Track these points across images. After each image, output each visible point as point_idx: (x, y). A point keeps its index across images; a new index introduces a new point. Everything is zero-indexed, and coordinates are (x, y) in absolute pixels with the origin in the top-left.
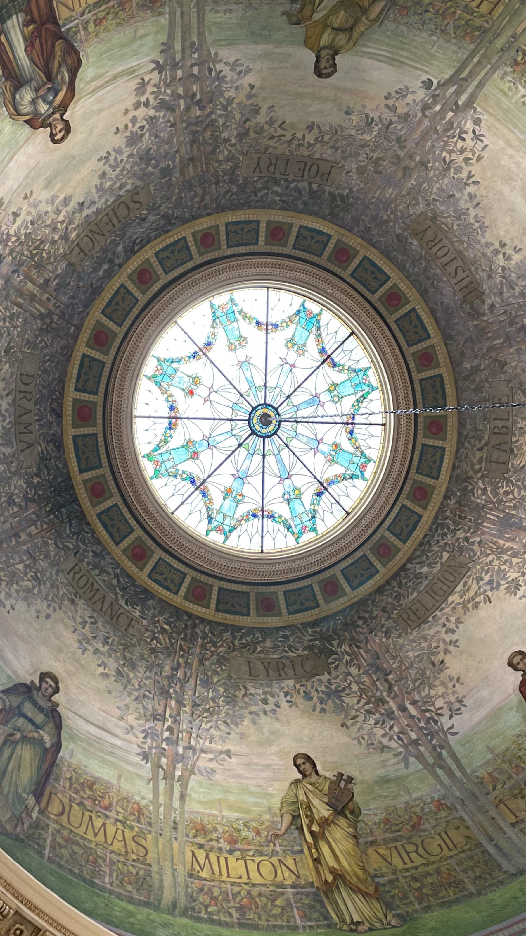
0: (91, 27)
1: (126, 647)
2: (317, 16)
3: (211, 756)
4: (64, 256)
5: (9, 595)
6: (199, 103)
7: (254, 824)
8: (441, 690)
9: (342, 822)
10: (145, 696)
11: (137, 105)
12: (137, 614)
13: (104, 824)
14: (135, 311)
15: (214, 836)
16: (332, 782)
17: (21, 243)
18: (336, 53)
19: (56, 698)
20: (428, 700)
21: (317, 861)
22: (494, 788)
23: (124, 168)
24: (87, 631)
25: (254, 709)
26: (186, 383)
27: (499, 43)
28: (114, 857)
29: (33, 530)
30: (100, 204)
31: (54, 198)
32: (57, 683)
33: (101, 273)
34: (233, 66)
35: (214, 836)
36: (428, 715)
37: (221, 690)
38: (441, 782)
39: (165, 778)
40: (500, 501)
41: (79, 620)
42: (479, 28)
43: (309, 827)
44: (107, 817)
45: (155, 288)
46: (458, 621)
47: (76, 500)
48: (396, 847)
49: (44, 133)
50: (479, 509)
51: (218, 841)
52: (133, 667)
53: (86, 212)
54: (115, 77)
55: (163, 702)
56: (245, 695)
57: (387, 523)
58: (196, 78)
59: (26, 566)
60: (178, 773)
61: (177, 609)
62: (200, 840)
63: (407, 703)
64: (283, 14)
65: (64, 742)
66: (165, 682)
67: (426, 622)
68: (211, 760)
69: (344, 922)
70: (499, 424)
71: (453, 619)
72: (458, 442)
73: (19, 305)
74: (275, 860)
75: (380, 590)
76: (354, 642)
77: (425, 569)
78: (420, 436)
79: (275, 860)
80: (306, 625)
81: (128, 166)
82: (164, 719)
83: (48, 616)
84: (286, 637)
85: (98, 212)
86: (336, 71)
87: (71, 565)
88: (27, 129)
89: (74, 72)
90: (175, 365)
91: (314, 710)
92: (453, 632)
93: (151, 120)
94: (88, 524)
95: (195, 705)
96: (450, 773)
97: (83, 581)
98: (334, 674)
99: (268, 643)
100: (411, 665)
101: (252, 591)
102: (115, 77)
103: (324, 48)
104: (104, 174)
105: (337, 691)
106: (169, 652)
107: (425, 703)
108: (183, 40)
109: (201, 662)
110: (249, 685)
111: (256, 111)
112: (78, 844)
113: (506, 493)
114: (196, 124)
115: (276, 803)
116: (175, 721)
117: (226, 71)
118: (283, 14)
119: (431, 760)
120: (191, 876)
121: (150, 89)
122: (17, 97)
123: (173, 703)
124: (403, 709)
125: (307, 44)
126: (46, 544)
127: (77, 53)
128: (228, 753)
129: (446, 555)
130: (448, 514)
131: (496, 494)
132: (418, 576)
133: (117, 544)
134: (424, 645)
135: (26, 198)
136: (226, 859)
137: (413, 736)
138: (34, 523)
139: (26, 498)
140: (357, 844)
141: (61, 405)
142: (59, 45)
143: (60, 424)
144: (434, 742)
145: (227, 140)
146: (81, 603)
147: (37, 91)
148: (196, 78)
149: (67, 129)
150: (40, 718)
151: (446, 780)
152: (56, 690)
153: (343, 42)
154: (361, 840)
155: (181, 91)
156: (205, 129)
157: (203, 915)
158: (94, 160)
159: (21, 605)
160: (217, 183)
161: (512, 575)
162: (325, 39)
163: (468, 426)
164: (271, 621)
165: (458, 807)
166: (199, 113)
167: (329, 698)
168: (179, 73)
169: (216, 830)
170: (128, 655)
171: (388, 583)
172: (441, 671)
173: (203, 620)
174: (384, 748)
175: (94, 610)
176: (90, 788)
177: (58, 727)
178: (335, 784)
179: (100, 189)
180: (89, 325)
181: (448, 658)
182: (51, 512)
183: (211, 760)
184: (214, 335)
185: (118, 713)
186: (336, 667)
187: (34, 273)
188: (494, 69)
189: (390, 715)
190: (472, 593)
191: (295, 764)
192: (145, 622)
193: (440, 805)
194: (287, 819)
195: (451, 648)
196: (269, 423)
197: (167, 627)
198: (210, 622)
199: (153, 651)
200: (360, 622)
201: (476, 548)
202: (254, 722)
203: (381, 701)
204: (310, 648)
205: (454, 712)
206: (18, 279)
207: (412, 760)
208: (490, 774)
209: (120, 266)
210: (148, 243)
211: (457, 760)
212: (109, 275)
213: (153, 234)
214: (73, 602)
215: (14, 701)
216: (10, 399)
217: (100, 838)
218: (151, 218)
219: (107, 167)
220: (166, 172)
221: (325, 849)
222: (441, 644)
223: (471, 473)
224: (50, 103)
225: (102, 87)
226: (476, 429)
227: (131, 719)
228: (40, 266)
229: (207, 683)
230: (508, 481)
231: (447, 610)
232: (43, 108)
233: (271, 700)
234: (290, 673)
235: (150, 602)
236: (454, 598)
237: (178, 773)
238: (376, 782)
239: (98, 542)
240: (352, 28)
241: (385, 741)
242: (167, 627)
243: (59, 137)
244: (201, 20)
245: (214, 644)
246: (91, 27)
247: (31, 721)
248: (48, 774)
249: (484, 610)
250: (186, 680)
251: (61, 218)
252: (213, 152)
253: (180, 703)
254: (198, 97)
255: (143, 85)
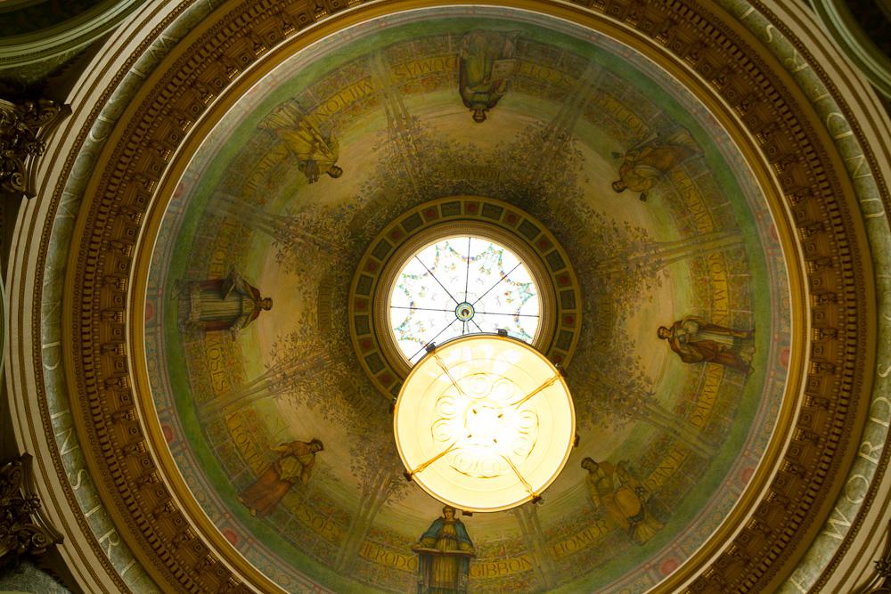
0: (695, 376)
1: (451, 162)
2: (615, 474)
3: (383, 142)
4: (611, 295)
5: (523, 140)
6: (620, 400)
7: (348, 124)
8: (291, 261)
9: (306, 158)
10: (429, 146)
11: (642, 374)
12: (454, 181)
13: (422, 71)
14: (560, 304)
15: (365, 104)
16: (319, 173)
17: (635, 280)
18: (591, 472)
19: (473, 113)
20: (294, 250)
21: (310, 128)
22: (242, 231)
23: (621, 348)
24: (474, 155)
25: (373, 181)
26: (511, 296)
27: (536, 543)
28: (412, 59)
29: (529, 177)
30: (616, 327)
31: (639, 309)
32: (476, 120)
33: (589, 304)
34: (623, 426)
35: (365, 104)
36: (290, 243)
37: (394, 177)
38: (267, 214)
39: (400, 115)
40: (331, 372)
41: (481, 156)
42: (550, 539)
43: (320, 143)
44: (423, 76)
45: (560, 320)
46: (305, 300)
47: (518, 206)
48: (274, 163)
49: (669, 324)
50: (337, 360)
51: (362, 103)
52: (442, 156)
53: (619, 318)
54: (663, 372)
55: (419, 150)
56: (381, 184)
57: (370, 318)
58: (630, 407)
59: (522, 159)
60: (395, 122)
61: (437, 198)
62: (370, 98)
63: (303, 241)
64: (629, 461)
65: (459, 95)
66: (422, 160)
67: (319, 288)
68: (382, 140)
69: (287, 106)
70: (362, 406)
71: (308, 299)
72: (371, 383)
73: (613, 258)
74: (331, 114)
75: (349, 285)
76: (344, 251)
77: (337, 312)
78: (389, 369)
79: (331, 114)
80: (372, 239)
81: (620, 351)
82: (414, 143)
83: (497, 146)
84: (377, 226)
85: (614, 324)
86: (582, 466)
87: (500, 177)
88: (678, 319)
89: (683, 357)
90: (523, 299)
91: (344, 203)
92: (304, 293)
93: (630, 375)
94: (505, 201)
95: (402, 161)
96: (265, 222)
97: (490, 174)
98: (344, 227)
99: (384, 217)
100: (312, 261)
101: (407, 235)
102: (663, 372)
103: (597, 469)
104: (627, 339)
105: (338, 220)
106: (429, 175)
107: (295, 248)
108: (654, 412)
109: (410, 183)
110: (382, 190)
111: (594, 422)
112: (433, 53)
113: (332, 379)
114: (611, 393)
115: (341, 143)
116: (408, 146)
117: (623, 421)
118: (629, 461)
119: (278, 221)
120: (369, 77)
121: (644, 384)
122: (696, 324)
123: (413, 153)
124: (303, 237)
125: (606, 462)
126: (519, 176)
127: (689, 362)
128: (375, 150)
129: (333, 327)
130: (347, 347)
131: (336, 374)
132: (337, 307)
133: (485, 204)
134: (312, 277)
135: (651, 298)
136: (354, 97)
137: (291, 227)
138: (531, 180)
139: (543, 187)
140: (293, 151)
141: (557, 238)
142: (700, 356)
143: (551, 231)
144: (280, 232)
145: (592, 400)
146: (485, 164)
147: (690, 335)
148: (630, 407)
149: (661, 337)
150: (477, 98)
151: (265, 217)
152: (474, 117)
153: (593, 478)
154: (293, 154)
155: (631, 396)
156: (605, 395)
157: (357, 61)
158: (637, 339)
159: (514, 140)
160: (577, 383)
161: (299, 343)
162: (601, 472)
163: (373, 393)
164: (388, 229)
165: (254, 208)
166: (615, 397)
167: (341, 215)
168: (640, 401)
169: (365, 108)
170: (448, 159)
171: (348, 291)
172: (297, 270)
173: (421, 203)
174: (302, 210)
175: (476, 166)
176: (436, 84)
177: (465, 101)
178: (317, 173)
179: (623, 332)
180: (575, 281)
181: (297, 279)
182: (526, 191)
183: (382, 140)
184: (518, 326)
185: (438, 129)
186: (345, 231)
187: (618, 276)
188: (525, 534)
189: (307, 229)
190: (309, 319)
191: (340, 169)
192: (448, 180)
193: (263, 202)
194: (332, 139)
195: (299, 285)
196: (468, 313)
197: (436, 186)
198: (418, 204)
199: (436, 170)
200: (348, 262)
201: (324, 342)
202: (370, 174)
203: (315, 233)
204: (363, 231)
205: (280, 255)
206: (623, 267)
207: (286, 215)
208: (248, 236)
209: (583, 314)
210: (581, 334)
211: (265, 231)
212: (585, 306)
213: (582, 339)
214: (489, 162)
215: (494, 96)
216: (583, 220)
217: (422, 64)
218: (590, 344)
219: (628, 342)
220: (602, 365)
221: (309, 138)
222: (305, 283)
223: (353, 373)
224: (679, 337)
225: (664, 364)
226: (369, 395)
227: (430, 131)
228: (618, 281)
229: (402, 175)
230: (335, 385)
231: (314, 302)
232: (680, 332)
233: (367, 191)
234: (365, 212)
235: (451, 192)
236: (315, 310)
237: (395, 122)
238: (297, 190)
239: (494, 197)
240: (596, 485)
241: (303, 214)
242: (436, 186)
243: (661, 331)
244: (656, 425)
245: (409, 196)
246: (695, 376)
247: (481, 93)
248: (461, 76)
249: (298, 315)
250: (413, 170)
251: (628, 306)
252: (593, 391)
253: (410, 156)
254: (622, 402)
255: (649, 381)
